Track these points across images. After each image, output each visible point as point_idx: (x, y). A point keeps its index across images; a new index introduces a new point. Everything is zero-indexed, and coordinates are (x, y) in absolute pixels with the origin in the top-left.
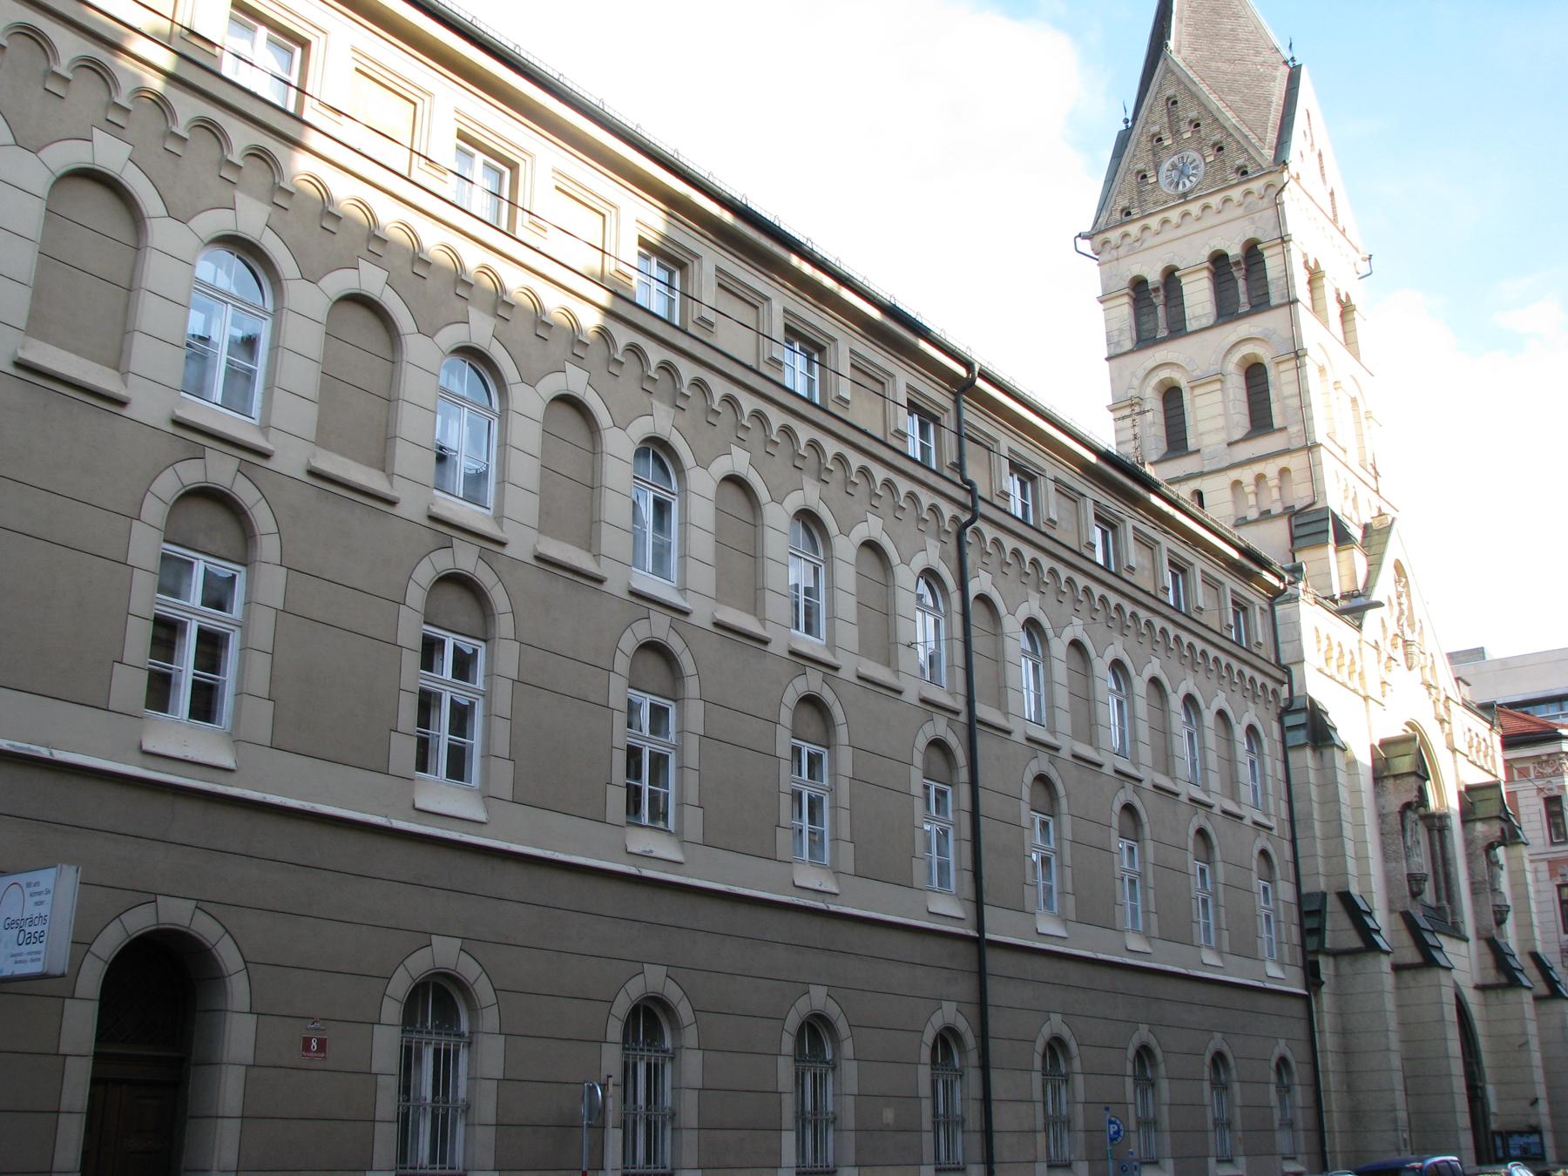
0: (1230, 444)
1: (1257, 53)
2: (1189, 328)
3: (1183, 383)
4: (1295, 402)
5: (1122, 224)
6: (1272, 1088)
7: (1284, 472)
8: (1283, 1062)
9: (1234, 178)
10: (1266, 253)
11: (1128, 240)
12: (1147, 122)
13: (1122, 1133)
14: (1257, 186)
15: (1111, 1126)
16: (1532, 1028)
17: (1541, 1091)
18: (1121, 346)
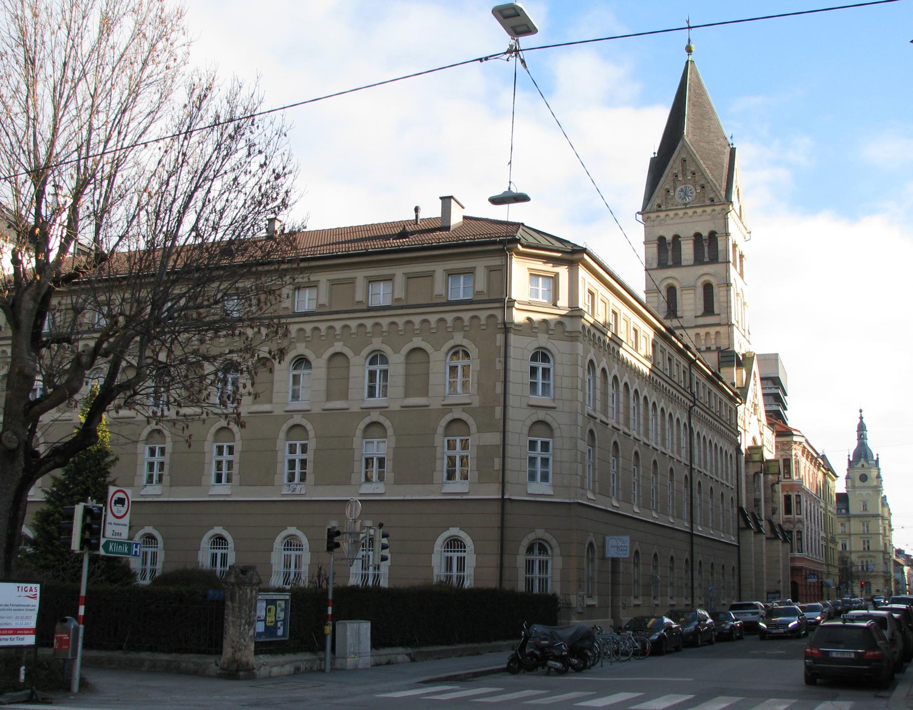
0: (696, 317)
2: (683, 264)
3: (678, 287)
4: (725, 305)
5: (657, 211)
6: (585, 559)
7: (717, 333)
8: (591, 545)
9: (708, 202)
10: (719, 239)
11: (659, 219)
12: (672, 167)
14: (718, 208)
16: (764, 549)
17: (781, 579)
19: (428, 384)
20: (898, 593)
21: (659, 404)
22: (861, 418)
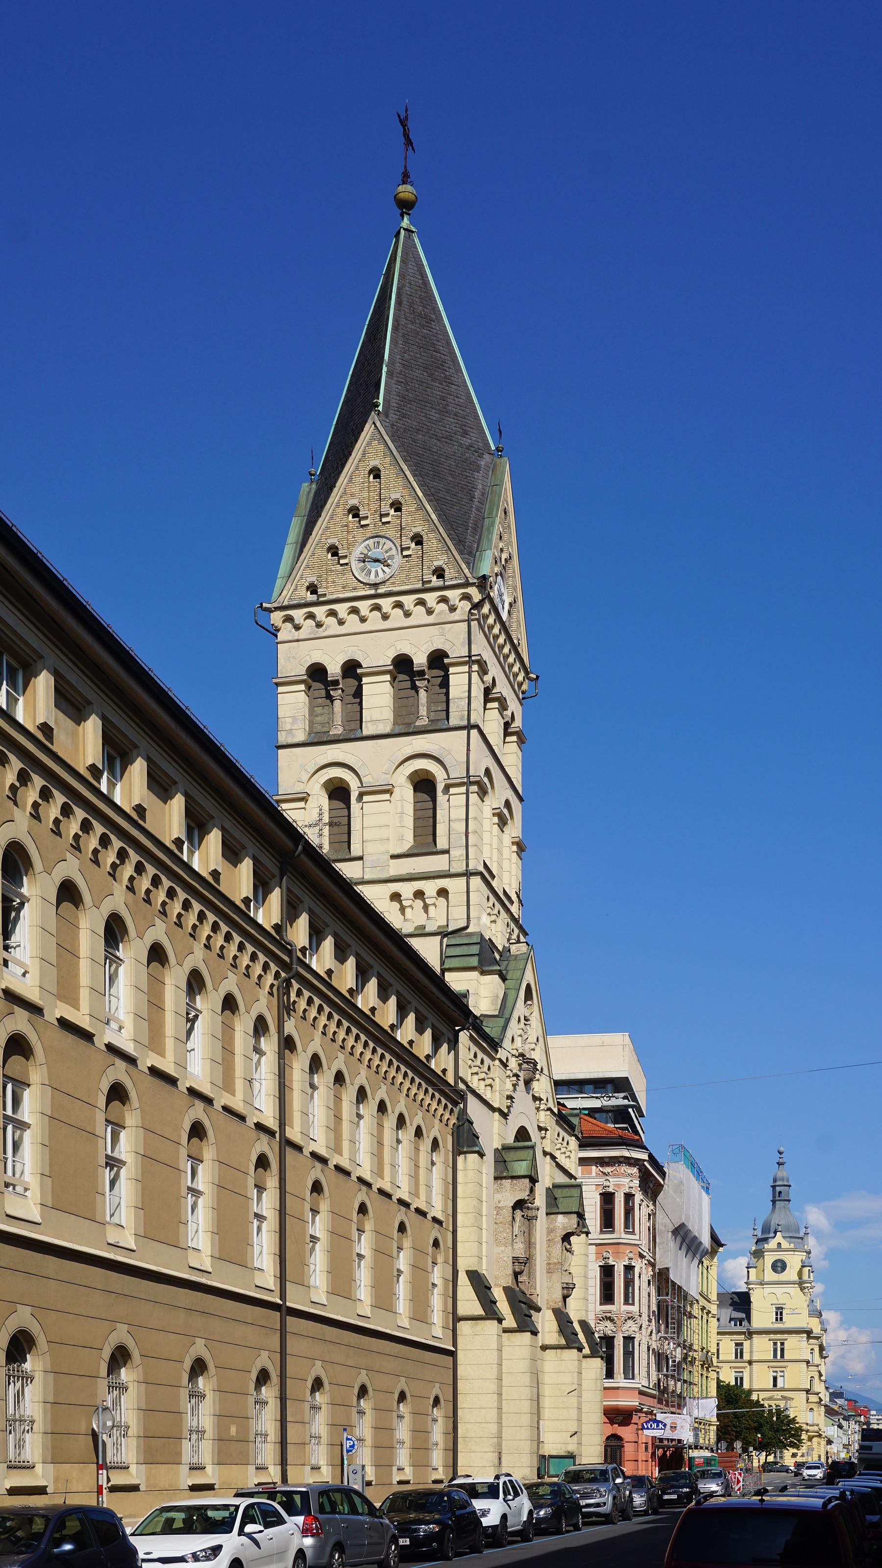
1: (465, 433)
12: (345, 493)
13: (356, 1447)
15: (348, 1442)
18: (293, 736)
19: (280, 1188)
20: (340, 1534)
21: (428, 1132)
22: (405, 167)
